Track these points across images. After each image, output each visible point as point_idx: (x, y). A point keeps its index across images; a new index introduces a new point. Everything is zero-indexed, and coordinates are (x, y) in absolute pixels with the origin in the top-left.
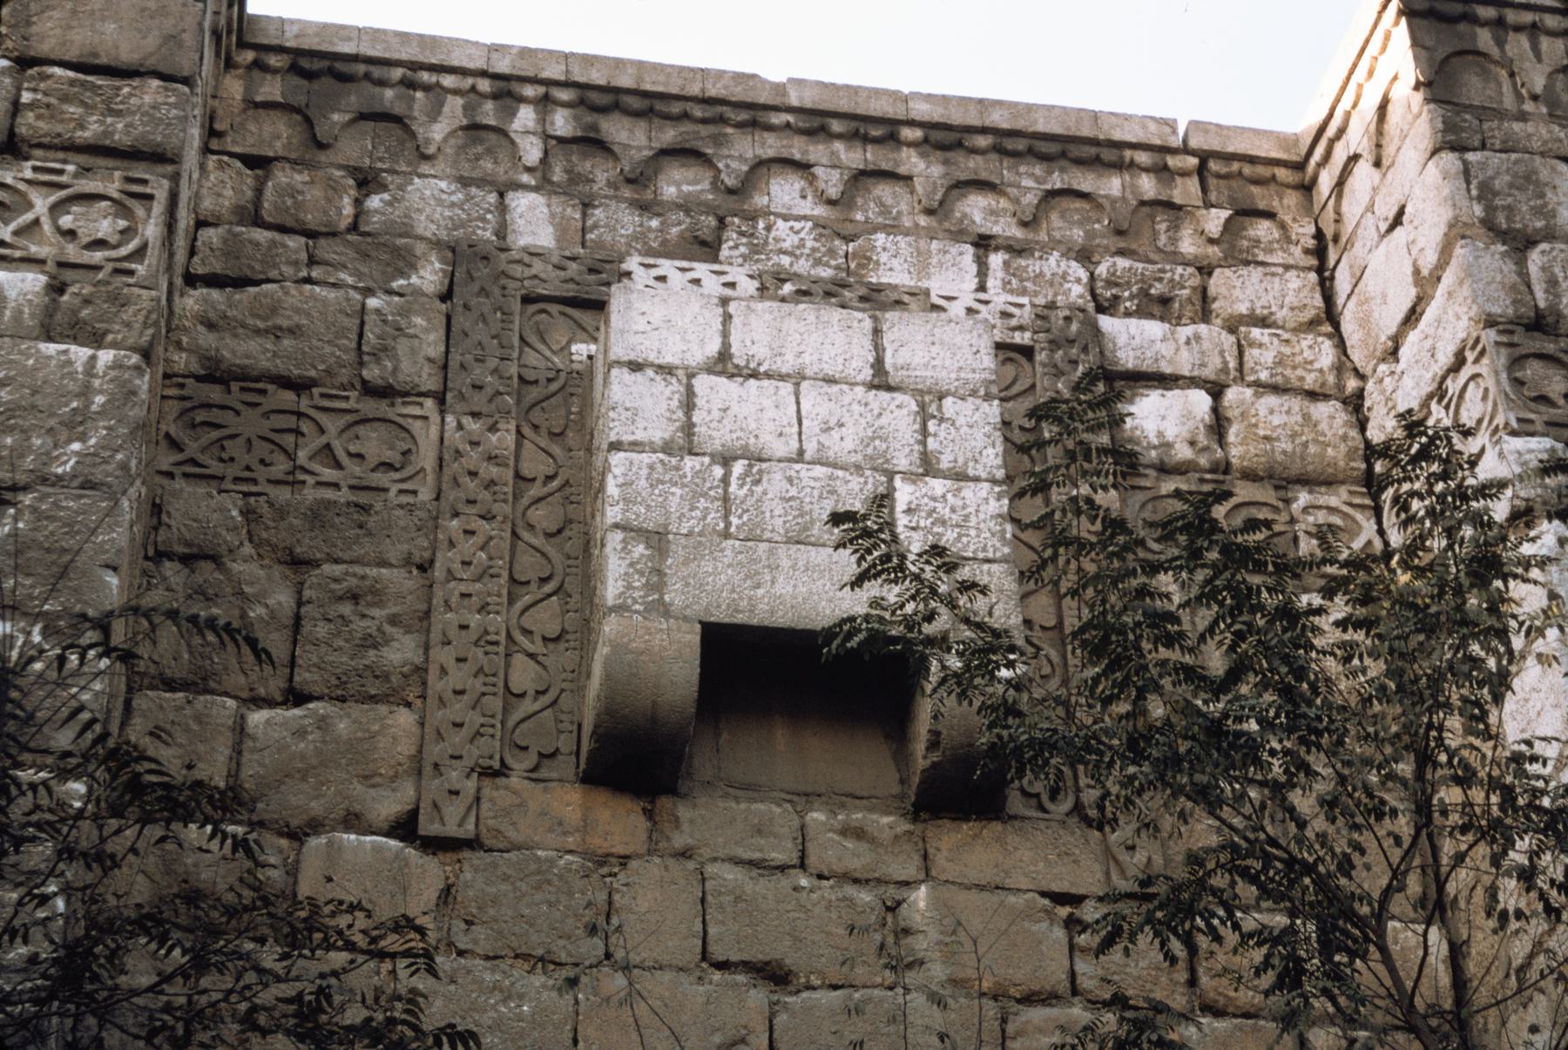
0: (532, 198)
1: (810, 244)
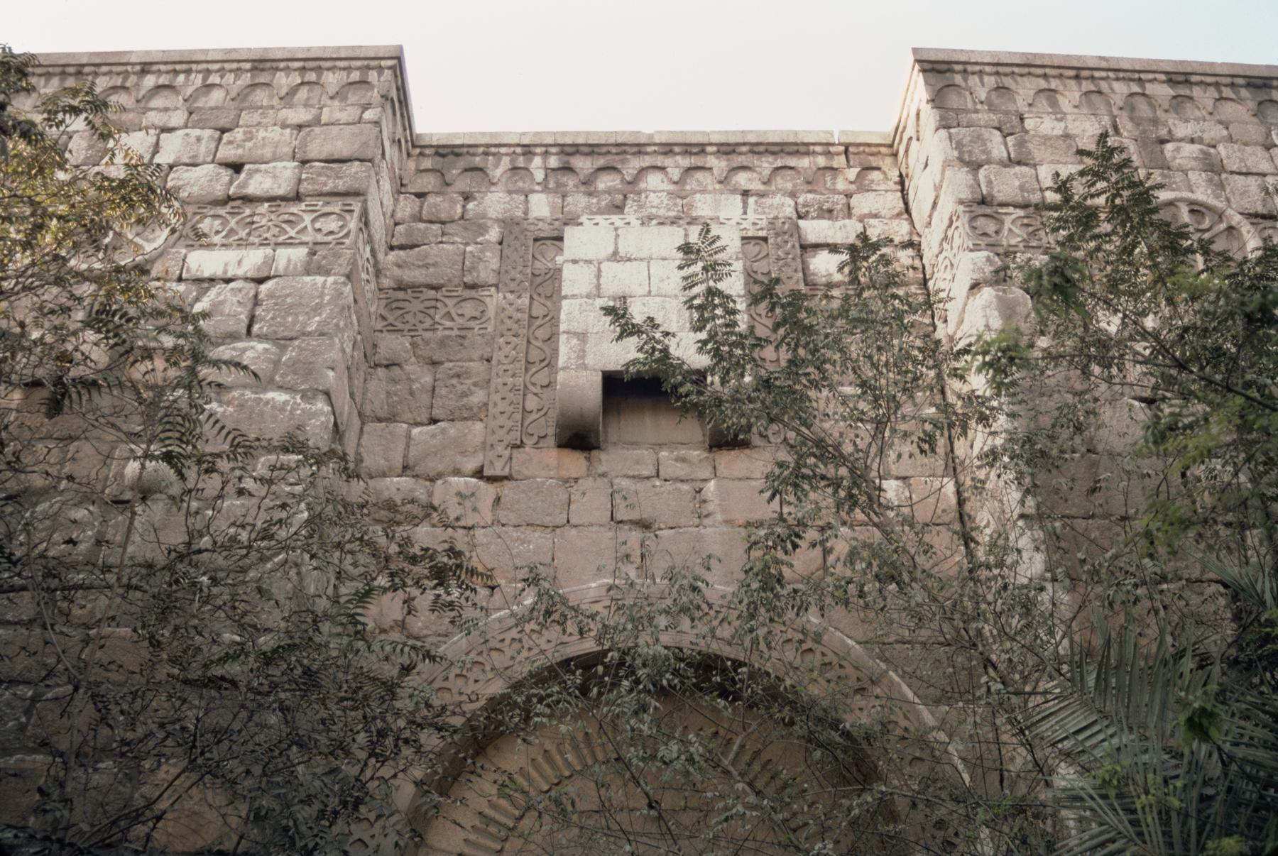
0: (542, 196)
1: (666, 202)
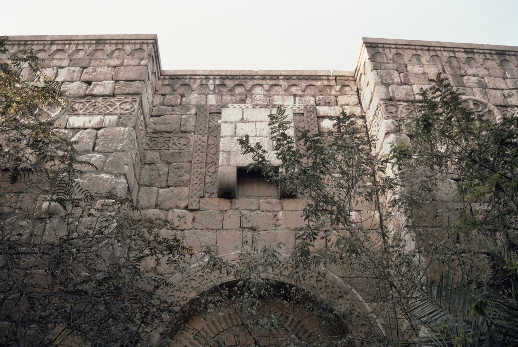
0: (213, 96)
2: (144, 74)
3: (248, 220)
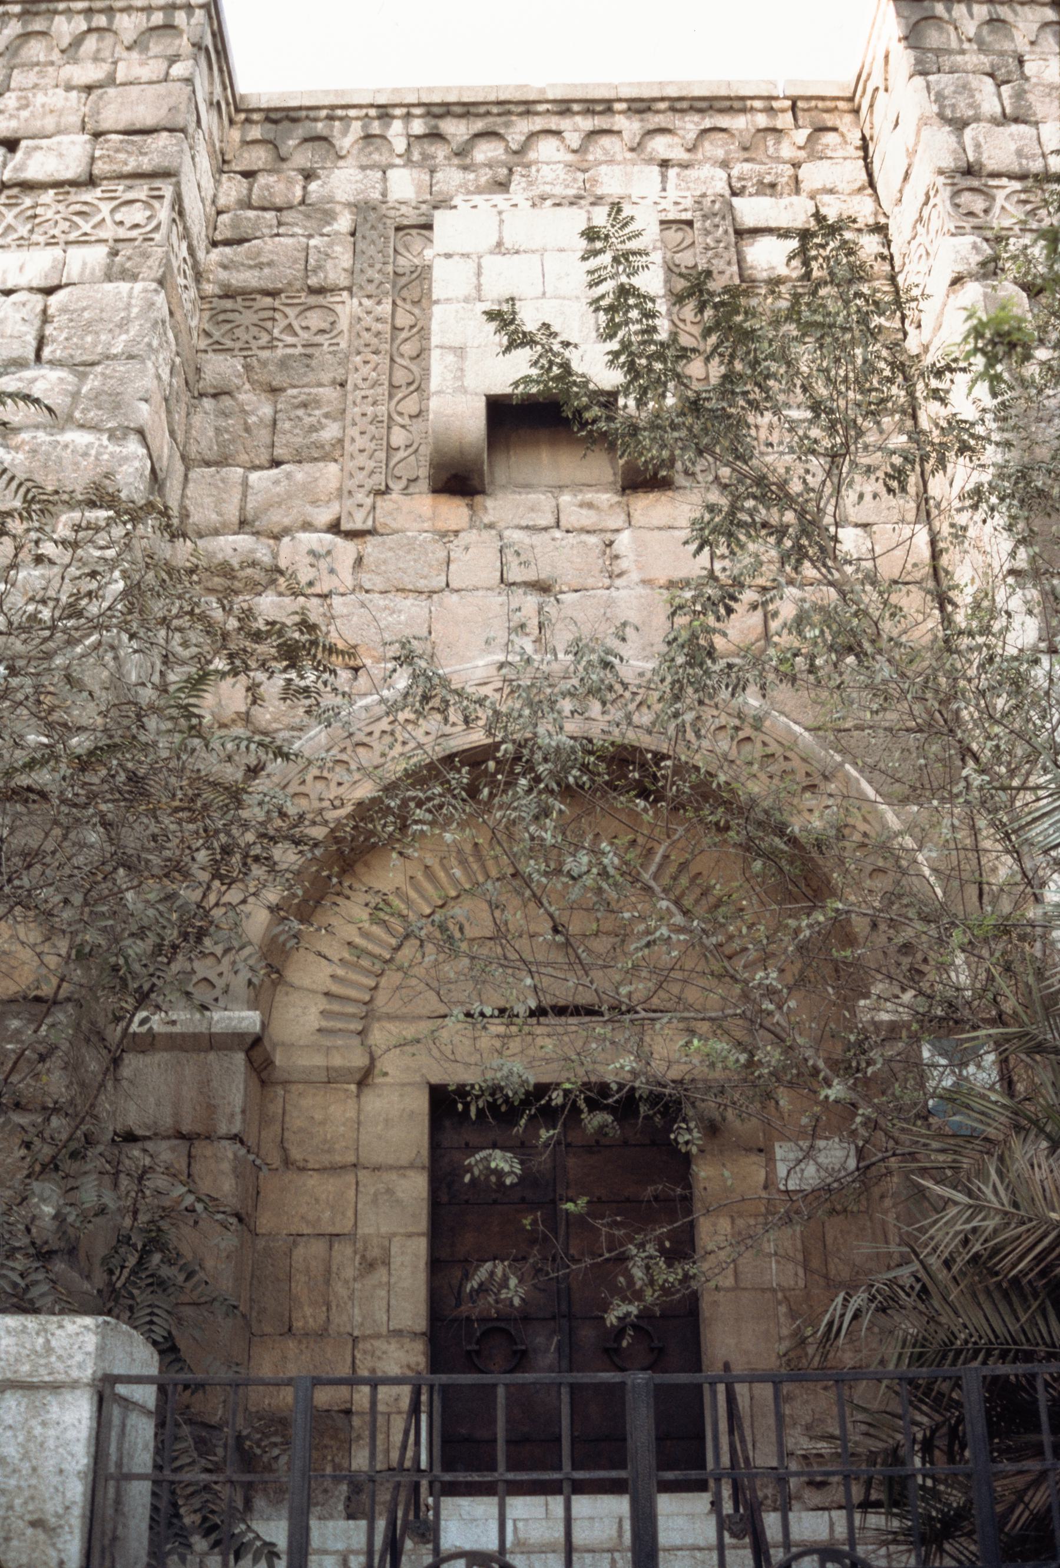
0: (405, 172)
1: (562, 176)
2: (183, 107)
3: (523, 558)
